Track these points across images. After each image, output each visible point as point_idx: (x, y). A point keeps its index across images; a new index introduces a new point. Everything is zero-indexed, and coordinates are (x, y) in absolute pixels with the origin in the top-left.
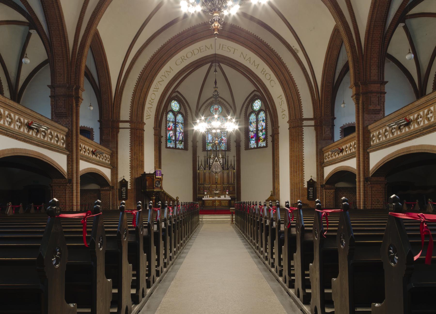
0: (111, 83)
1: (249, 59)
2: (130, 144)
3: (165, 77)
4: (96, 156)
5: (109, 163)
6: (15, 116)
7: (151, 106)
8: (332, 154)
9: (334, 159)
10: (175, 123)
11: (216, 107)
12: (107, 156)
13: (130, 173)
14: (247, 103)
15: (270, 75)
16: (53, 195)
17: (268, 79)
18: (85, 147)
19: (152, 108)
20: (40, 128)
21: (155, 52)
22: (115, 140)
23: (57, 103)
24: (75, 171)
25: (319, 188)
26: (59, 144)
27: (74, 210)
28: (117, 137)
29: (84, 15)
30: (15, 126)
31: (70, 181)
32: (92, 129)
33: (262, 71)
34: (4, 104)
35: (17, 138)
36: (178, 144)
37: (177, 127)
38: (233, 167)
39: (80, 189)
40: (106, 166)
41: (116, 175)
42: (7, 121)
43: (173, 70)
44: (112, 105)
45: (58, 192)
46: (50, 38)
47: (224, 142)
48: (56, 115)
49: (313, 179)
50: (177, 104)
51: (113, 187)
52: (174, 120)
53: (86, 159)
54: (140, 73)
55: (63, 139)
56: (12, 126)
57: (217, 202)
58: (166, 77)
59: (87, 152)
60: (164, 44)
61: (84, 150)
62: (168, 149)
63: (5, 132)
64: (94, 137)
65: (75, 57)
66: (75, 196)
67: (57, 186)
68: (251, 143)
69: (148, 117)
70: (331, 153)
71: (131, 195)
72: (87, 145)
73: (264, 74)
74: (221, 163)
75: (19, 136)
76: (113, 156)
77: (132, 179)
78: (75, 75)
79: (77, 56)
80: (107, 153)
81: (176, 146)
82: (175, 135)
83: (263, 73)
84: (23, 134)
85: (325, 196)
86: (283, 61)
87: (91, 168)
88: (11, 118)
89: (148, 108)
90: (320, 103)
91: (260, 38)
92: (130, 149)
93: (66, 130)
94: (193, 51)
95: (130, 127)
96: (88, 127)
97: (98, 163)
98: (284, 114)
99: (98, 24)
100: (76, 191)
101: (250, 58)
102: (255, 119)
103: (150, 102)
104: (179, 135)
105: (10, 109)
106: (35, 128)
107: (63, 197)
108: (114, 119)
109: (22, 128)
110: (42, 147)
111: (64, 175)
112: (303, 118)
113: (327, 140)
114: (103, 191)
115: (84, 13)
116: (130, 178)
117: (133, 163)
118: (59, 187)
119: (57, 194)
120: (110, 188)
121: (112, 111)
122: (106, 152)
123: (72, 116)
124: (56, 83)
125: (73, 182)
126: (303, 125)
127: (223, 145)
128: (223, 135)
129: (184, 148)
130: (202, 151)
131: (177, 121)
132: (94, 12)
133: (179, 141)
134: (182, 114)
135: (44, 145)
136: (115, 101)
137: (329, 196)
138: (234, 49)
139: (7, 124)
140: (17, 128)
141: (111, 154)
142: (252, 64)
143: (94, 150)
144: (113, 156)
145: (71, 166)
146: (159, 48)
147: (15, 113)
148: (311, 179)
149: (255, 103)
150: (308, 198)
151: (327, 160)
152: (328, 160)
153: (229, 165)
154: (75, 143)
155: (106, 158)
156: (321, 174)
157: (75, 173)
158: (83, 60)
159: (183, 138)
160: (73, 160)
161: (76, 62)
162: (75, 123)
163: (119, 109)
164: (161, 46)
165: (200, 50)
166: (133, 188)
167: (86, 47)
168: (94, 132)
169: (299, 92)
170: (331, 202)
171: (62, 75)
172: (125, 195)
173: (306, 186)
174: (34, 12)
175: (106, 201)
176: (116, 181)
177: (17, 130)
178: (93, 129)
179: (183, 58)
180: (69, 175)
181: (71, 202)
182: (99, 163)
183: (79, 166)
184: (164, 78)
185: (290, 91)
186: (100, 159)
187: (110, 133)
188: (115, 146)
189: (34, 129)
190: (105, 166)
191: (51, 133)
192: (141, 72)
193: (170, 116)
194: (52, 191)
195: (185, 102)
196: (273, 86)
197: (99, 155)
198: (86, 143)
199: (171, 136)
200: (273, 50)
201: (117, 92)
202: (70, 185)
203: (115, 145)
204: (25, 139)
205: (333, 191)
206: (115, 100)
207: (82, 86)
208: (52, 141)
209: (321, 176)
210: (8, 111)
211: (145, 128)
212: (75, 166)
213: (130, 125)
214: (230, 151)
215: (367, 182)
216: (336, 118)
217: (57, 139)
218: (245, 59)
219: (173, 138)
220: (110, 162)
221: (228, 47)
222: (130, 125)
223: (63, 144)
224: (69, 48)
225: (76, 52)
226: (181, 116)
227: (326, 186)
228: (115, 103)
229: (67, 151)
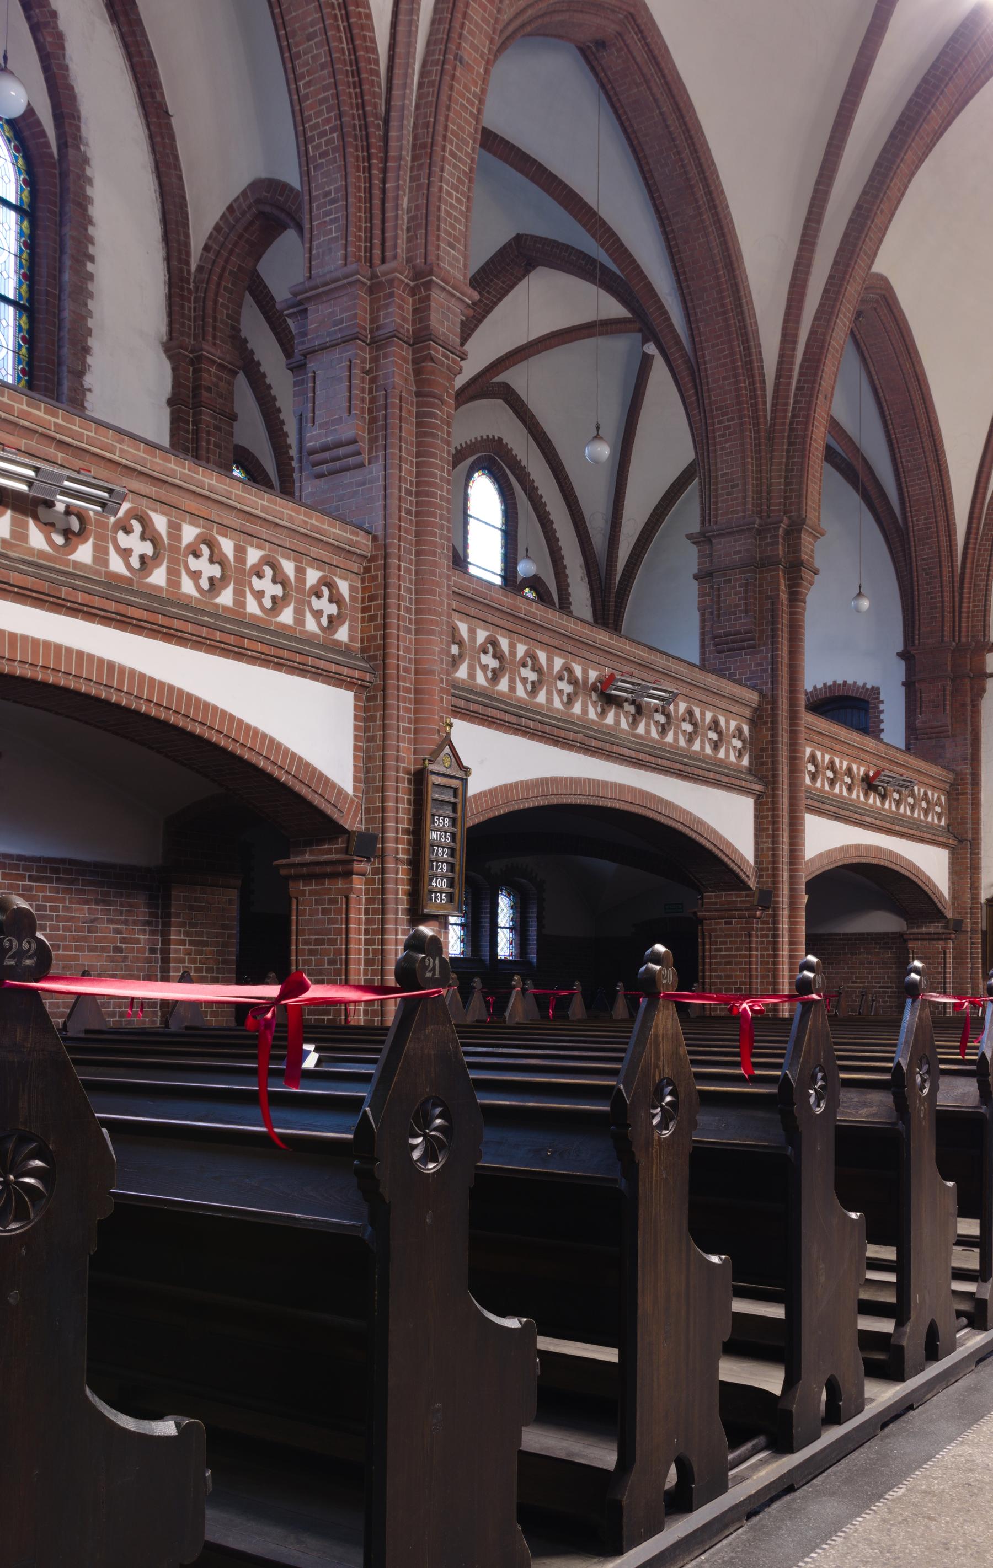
0: (951, 493)
4: (883, 797)
5: (943, 823)
6: (550, 660)
12: (933, 795)
16: (707, 953)
18: (832, 763)
20: (644, 697)
22: (969, 728)
23: (719, 597)
24: (786, 860)
26: (722, 755)
27: (781, 1015)
29: (817, 230)
30: (475, 670)
31: (767, 899)
32: (876, 691)
34: (511, 619)
35: (556, 741)
39: (807, 935)
40: (929, 836)
41: (972, 874)
42: (524, 680)
44: (957, 585)
45: (721, 943)
46: (695, 350)
48: (715, 645)
51: (958, 925)
53: (837, 810)
55: (739, 733)
56: (541, 698)
59: (842, 780)
61: (830, 774)
63: (514, 719)
64: (882, 721)
65: (787, 404)
66: (786, 960)
67: (721, 917)
72: (843, 754)
75: (562, 733)
76: (957, 794)
78: (786, 478)
79: (792, 401)
80: (931, 782)
84: (582, 725)
87: (857, 847)
88: (536, 668)
93: (754, 697)
96: (860, 683)
97: (888, 825)
99: (875, 254)
100: (791, 936)
105: (533, 634)
106: (626, 700)
107: (740, 963)
108: (964, 640)
109: (541, 689)
110: (655, 769)
111: (741, 874)
114: (917, 939)
115: (819, 221)
118: (726, 923)
119: (720, 950)
120: (946, 927)
121: (957, 609)
122: (926, 780)
123: (773, 644)
124: (716, 523)
125: (777, 902)
132: (858, 207)
135: (660, 761)
136: (968, 565)
139: (520, 692)
140: (557, 703)
141: (952, 785)
143: (871, 774)
144: (957, 794)
145: (770, 840)
147: (552, 649)
154: (785, 748)
155: (928, 802)
157: (785, 867)
158: (818, 410)
160: (777, 816)
161: (791, 424)
162: (785, 669)
163: (986, 596)
167: (829, 356)
168: (882, 702)
171: (737, 485)
174: (638, 266)
176: (973, 898)
177: (558, 710)
178: (878, 688)
180: (761, 876)
181: (769, 983)
182: (893, 827)
183: (803, 838)
186: (902, 810)
187: (944, 700)
188: (969, 751)
189: (626, 704)
190: (925, 835)
191: (690, 713)
194: (703, 938)
197: (898, 792)
198: (837, 747)
201: (974, 526)
202: (768, 916)
203: (969, 746)
204: (587, 741)
206: (969, 562)
207: (811, 516)
208: (696, 746)
210: (526, 644)
212: (785, 837)
217: (714, 736)
220: (949, 819)
223: (740, 755)
224: (762, 375)
225: (789, 384)
228: (968, 571)
229: (754, 779)
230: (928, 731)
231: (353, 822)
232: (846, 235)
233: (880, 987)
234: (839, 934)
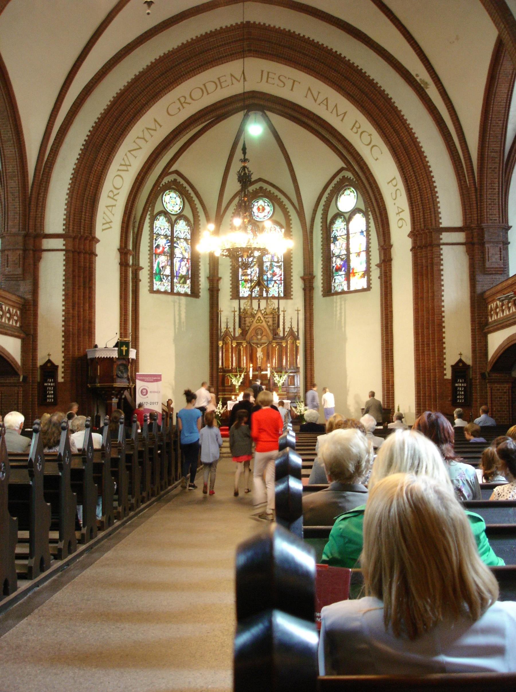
1: (325, 102)
2: (64, 285)
7: (113, 202)
8: (503, 305)
9: (507, 315)
10: (172, 240)
11: (261, 203)
12: (13, 311)
13: (63, 347)
14: (327, 196)
15: (370, 135)
17: (367, 143)
19: (115, 206)
21: (120, 90)
25: (478, 381)
33: (354, 126)
36: (178, 285)
37: (176, 247)
38: (296, 333)
40: (10, 332)
43: (161, 126)
49: (464, 359)
52: (169, 233)
54: (89, 134)
58: (147, 141)
62: (155, 295)
69: (107, 226)
70: (501, 303)
73: (357, 133)
74: (269, 324)
81: (172, 288)
82: (172, 265)
85: (491, 398)
86: (396, 105)
89: (107, 207)
90: (476, 195)
91: (345, 57)
92: (63, 295)
94: (204, 85)
98: (401, 219)
101: (327, 99)
103: (111, 195)
108: (31, 231)
112: (441, 226)
113: (492, 274)
114: (4, 386)
116: (64, 357)
117: (69, 326)
126: (441, 242)
129: (191, 292)
130: (231, 299)
131: (175, 234)
133: (179, 278)
134: (186, 219)
137: (500, 398)
138: (292, 81)
142: (331, 112)
146: (130, 81)
148: (460, 361)
151: (493, 319)
152: (495, 317)
153: (287, 329)
156: (481, 350)
159: (188, 271)
164: (133, 77)
166: (69, 379)
170: (504, 411)
172: (52, 396)
173: (448, 374)
179: (182, 100)
184: (141, 142)
185: (413, 168)
192: (90, 131)
193: (161, 224)
195: (193, 195)
199: (162, 267)
200: (375, 82)
205: (507, 386)
211: (99, 248)
214: (292, 299)
216: (511, 227)
218: (315, 101)
219: (168, 271)
220: (21, 323)
221: (279, 77)
222: (64, 242)
226: (184, 223)
227: (493, 375)
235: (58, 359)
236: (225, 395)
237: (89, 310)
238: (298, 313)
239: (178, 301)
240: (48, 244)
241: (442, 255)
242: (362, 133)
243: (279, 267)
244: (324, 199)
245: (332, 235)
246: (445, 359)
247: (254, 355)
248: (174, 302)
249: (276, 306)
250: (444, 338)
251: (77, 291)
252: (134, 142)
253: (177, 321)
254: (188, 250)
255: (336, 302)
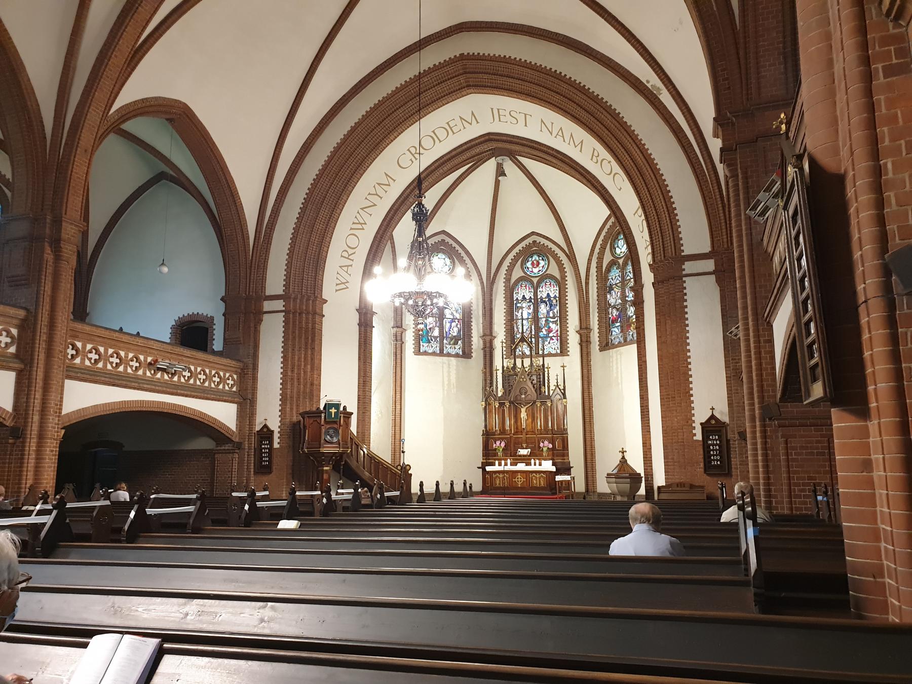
1: (560, 133)
3: (378, 196)
19: (351, 266)
28: (257, 332)
32: (212, 318)
36: (449, 346)
47: (555, 335)
50: (444, 259)
51: (239, 446)
57: (519, 476)
60: (355, 123)
68: (614, 333)
71: (281, 464)
73: (597, 163)
76: (244, 374)
77: (283, 424)
81: (442, 350)
83: (595, 159)
95: (284, 309)
102: (619, 276)
103: (345, 254)
104: (451, 326)
108: (251, 293)
112: (683, 254)
116: (280, 422)
126: (684, 273)
127: (551, 341)
128: (552, 320)
144: (244, 374)
149: (619, 240)
150: (708, 468)
156: (738, 403)
159: (459, 331)
165: (449, 129)
168: (215, 324)
169: (669, 191)
173: (699, 437)
175: (225, 477)
196: (621, 188)
199: (430, 329)
209: (738, 406)
213: (284, 303)
214: (569, 355)
215: (770, 419)
219: (436, 333)
222: (284, 303)
230: (231, 340)
231: (236, 439)
232: (94, 66)
233: (202, 480)
234: (183, 450)
235: (275, 425)
236: (489, 459)
237: (310, 372)
238: (564, 370)
239: (447, 362)
240: (267, 306)
241: (685, 288)
242: (602, 161)
243: (555, 322)
244: (598, 246)
245: (608, 284)
246: (693, 415)
247: (518, 415)
248: (443, 363)
249: (541, 363)
250: (692, 389)
251: (297, 353)
252: (366, 198)
253: (446, 383)
254: (460, 311)
255: (612, 357)
